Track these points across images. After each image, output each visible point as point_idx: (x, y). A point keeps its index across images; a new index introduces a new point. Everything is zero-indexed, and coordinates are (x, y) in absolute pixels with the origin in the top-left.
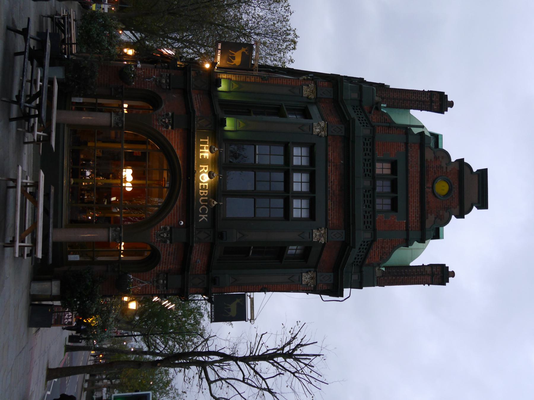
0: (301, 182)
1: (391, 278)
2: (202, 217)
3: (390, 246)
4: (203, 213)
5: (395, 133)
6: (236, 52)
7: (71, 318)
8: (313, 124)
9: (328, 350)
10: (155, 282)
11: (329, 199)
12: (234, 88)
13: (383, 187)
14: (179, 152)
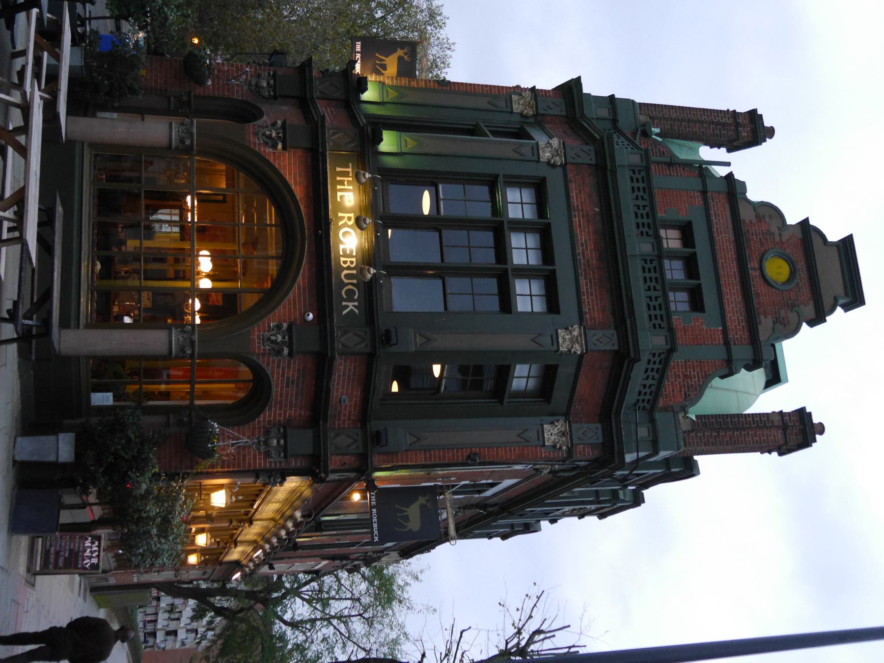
1: (709, 434)
2: (347, 306)
3: (729, 270)
4: (350, 298)
5: (681, 176)
6: (387, 57)
7: (96, 556)
9: (592, 638)
10: (262, 443)
11: (582, 275)
12: (390, 97)
13: (675, 271)
14: (298, 190)
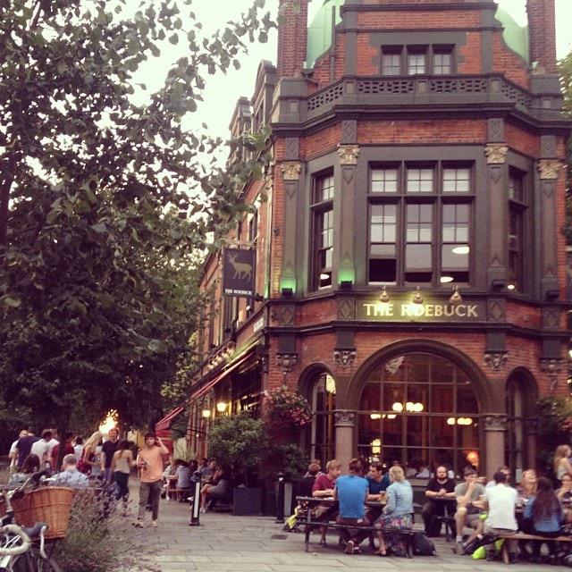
0: (384, 181)
6: (235, 271)
8: (342, 165)
14: (386, 342)
